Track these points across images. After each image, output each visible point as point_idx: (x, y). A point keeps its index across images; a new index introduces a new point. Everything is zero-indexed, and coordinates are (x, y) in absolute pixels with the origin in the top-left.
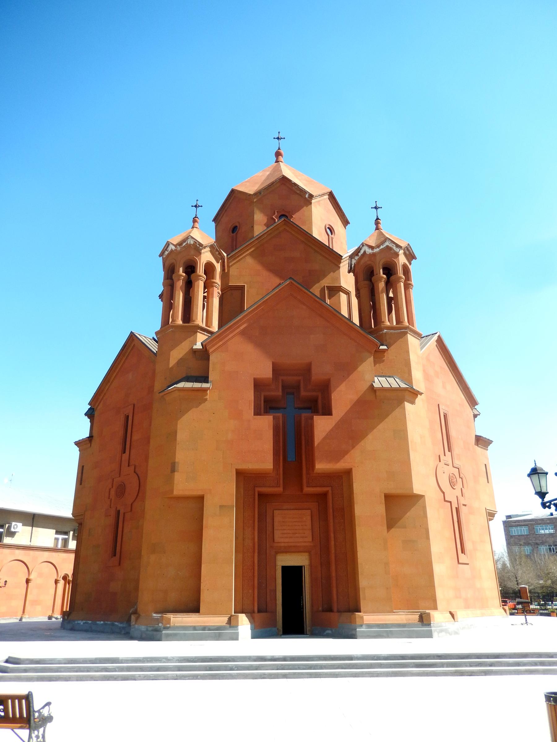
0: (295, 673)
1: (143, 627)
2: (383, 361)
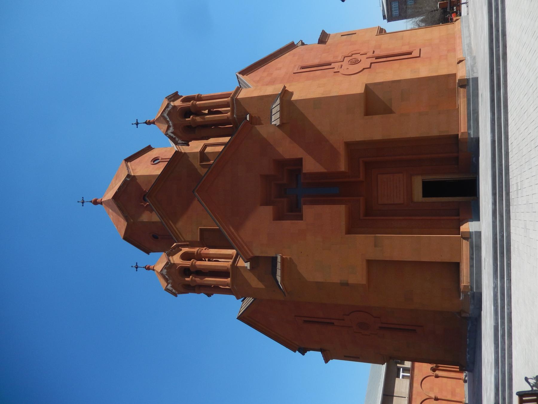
2: (259, 117)
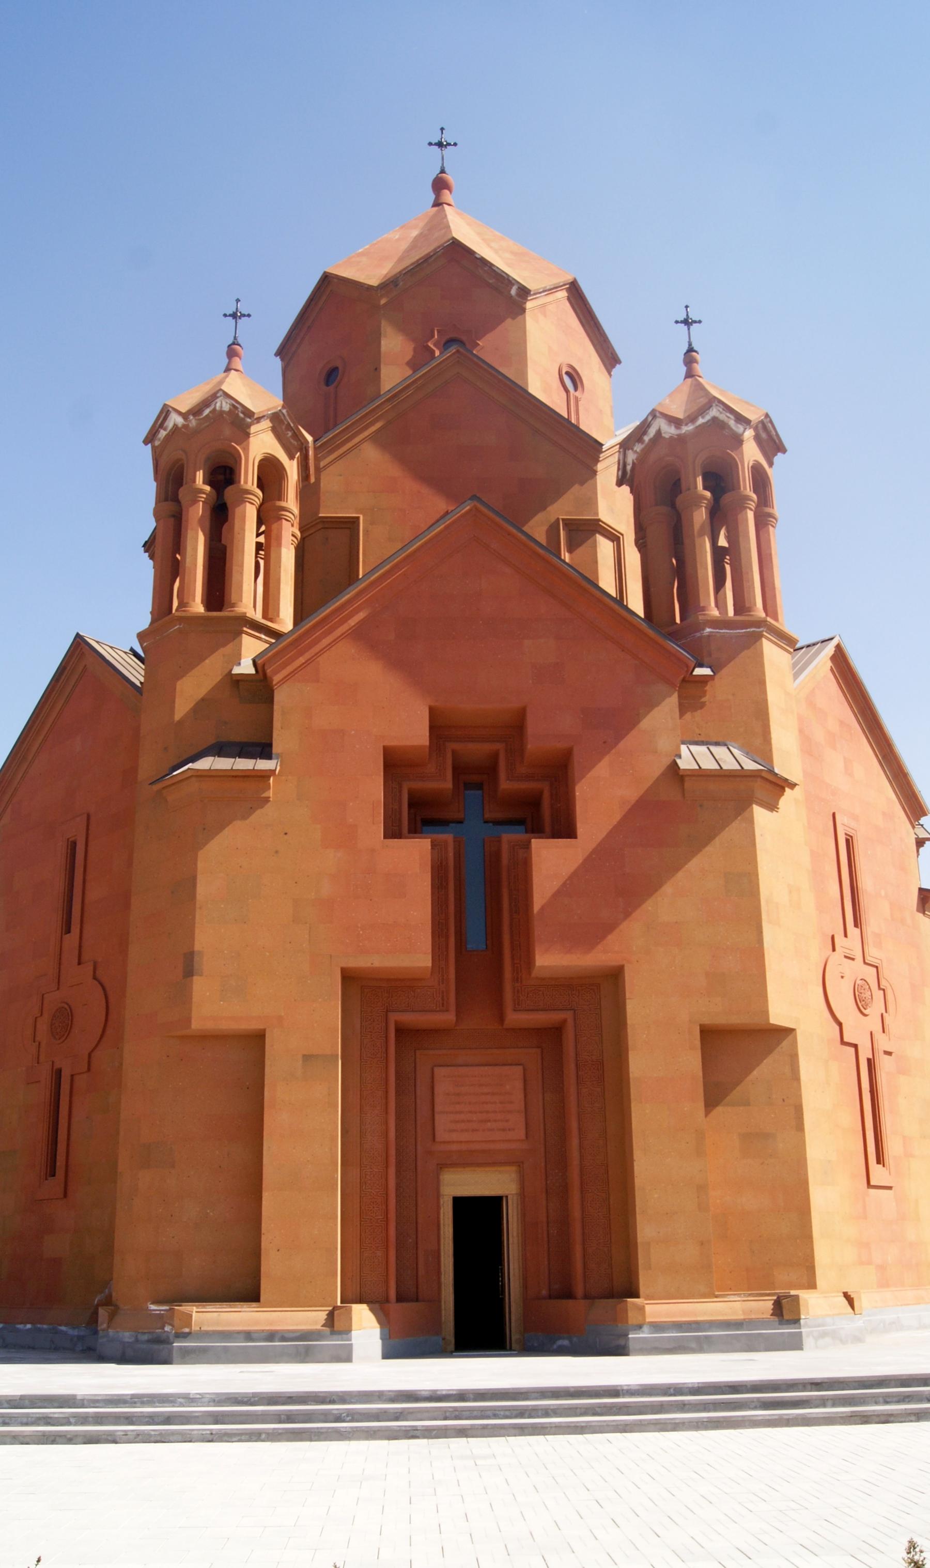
0: (485, 1427)
1: (127, 1334)
2: (702, 706)
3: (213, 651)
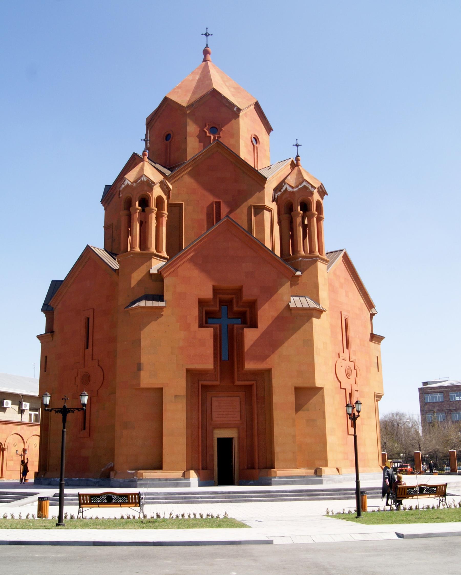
0: (236, 500)
1: (121, 480)
2: (298, 284)
3: (143, 264)
